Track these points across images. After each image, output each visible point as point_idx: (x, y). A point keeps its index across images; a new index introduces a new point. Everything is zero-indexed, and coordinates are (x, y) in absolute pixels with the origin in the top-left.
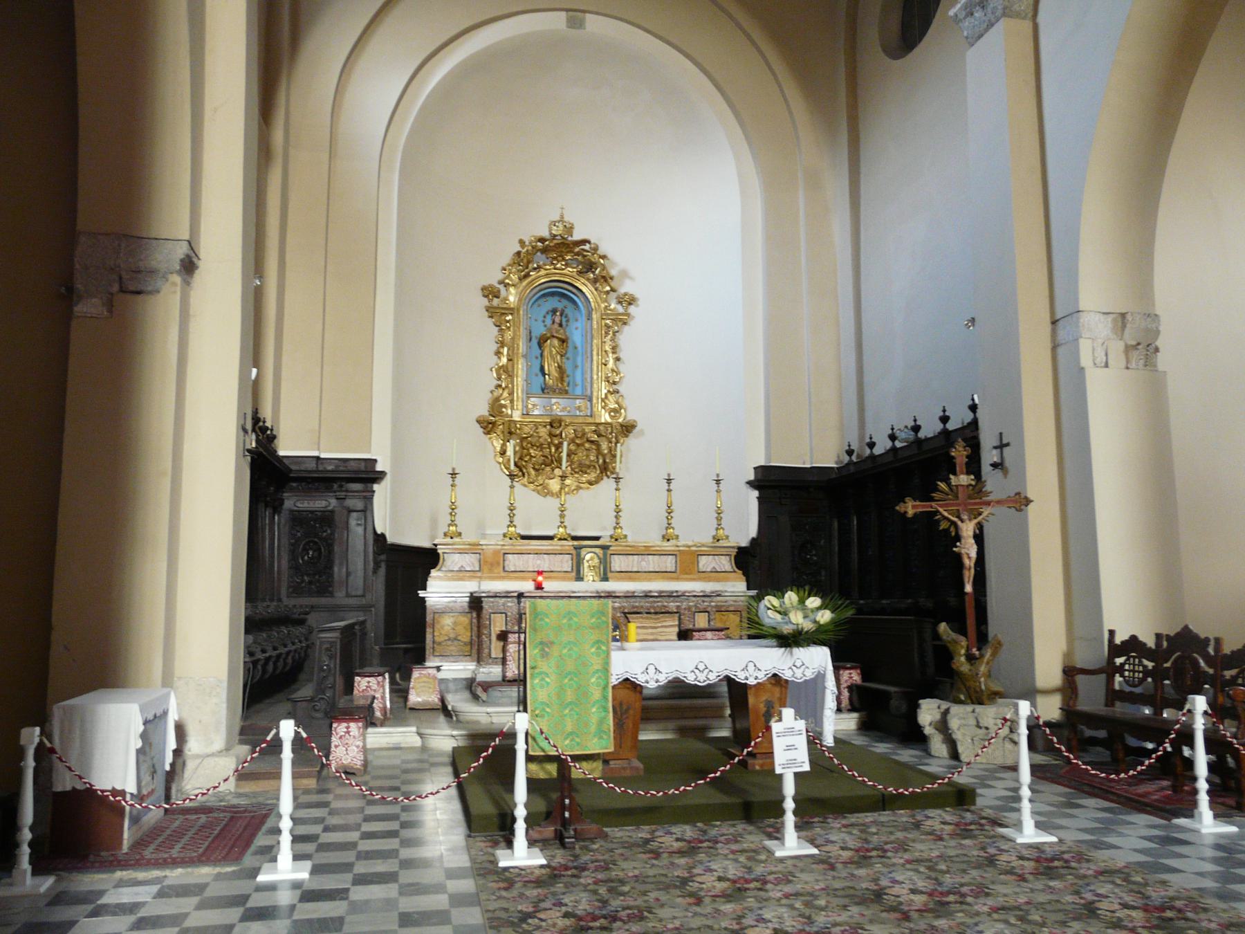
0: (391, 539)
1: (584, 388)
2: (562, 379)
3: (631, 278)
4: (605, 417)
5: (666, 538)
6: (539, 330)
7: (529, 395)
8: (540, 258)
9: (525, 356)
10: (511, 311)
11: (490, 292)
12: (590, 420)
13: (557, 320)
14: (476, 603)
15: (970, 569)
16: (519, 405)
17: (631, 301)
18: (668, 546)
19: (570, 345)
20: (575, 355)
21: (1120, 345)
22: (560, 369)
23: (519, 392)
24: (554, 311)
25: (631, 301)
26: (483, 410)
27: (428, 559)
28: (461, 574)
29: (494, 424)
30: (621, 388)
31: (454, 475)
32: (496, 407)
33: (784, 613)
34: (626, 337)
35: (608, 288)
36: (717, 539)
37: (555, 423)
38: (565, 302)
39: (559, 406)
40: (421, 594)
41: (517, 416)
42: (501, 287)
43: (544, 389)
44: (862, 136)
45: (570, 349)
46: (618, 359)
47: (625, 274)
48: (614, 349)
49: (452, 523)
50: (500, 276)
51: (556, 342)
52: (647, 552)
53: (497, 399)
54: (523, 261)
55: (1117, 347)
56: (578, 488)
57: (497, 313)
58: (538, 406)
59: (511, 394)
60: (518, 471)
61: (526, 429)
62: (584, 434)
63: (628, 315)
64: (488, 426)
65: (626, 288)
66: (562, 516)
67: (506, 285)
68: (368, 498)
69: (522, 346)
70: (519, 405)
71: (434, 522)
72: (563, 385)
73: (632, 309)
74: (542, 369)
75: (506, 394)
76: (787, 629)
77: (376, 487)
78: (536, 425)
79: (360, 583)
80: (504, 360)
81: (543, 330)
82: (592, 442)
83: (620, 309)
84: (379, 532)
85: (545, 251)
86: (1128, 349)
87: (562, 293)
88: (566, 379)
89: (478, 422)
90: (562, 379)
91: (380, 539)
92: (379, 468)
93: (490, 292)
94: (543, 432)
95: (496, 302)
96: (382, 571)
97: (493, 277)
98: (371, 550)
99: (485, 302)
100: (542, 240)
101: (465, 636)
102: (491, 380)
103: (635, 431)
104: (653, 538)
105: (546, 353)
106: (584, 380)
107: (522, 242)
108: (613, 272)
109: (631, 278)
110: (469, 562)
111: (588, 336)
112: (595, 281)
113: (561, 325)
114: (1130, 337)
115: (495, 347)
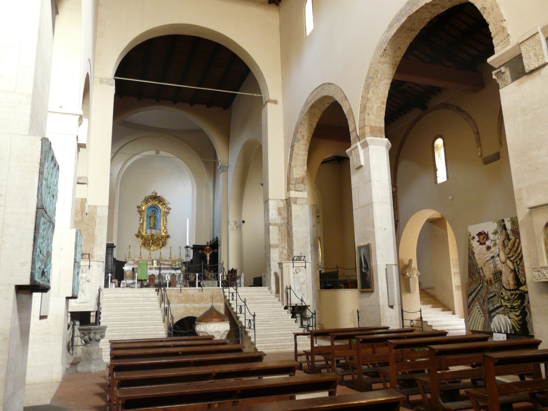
0: (117, 259)
1: (159, 228)
2: (154, 226)
3: (170, 204)
4: (163, 234)
5: (170, 258)
6: (150, 215)
7: (147, 229)
8: (150, 200)
9: (146, 221)
10: (143, 211)
11: (139, 207)
12: (160, 235)
13: (154, 213)
14: (133, 269)
15: (41, 237)
16: (144, 231)
17: (170, 209)
18: (170, 260)
19: (156, 218)
20: (158, 220)
21: (236, 227)
22: (154, 224)
23: (144, 229)
24: (153, 211)
25: (170, 209)
26: (137, 233)
27: (123, 264)
28: (131, 264)
29: (139, 236)
30: (167, 228)
31: (130, 246)
32: (139, 232)
33: (176, 266)
34: (169, 217)
35: (165, 206)
36: (179, 258)
37: (152, 235)
38: (155, 209)
39: (154, 231)
40: (123, 268)
41: (144, 234)
42: (141, 206)
43: (151, 228)
44: (216, 179)
45: (157, 219)
46: (167, 222)
47: (169, 203)
48: (166, 219)
49: (129, 255)
50: (141, 203)
51: (153, 218)
52: (166, 261)
53: (140, 230)
54: (146, 200)
55: (235, 227)
56: (157, 249)
57: (140, 212)
58: (149, 231)
59: (143, 229)
60: (144, 244)
61: (146, 237)
62: (158, 238)
63: (169, 212)
64: (137, 236)
65: (169, 206)
66: (150, 254)
67: (142, 206)
68: (112, 251)
69: (145, 218)
70: (144, 231)
71: (126, 256)
72: (154, 227)
73: (170, 211)
74: (150, 223)
75: (142, 229)
76: (176, 268)
77: (114, 249)
78: (148, 236)
79: (110, 267)
80: (142, 222)
81: (150, 215)
82: (160, 240)
83: (167, 211)
84: (114, 258)
85: (151, 198)
86: (237, 227)
87: (154, 209)
88: (155, 226)
89: (136, 235)
90: (154, 226)
91: (115, 259)
92: (114, 245)
93: (139, 207)
94: (150, 237)
95: (140, 209)
96: (115, 265)
97: (139, 204)
98: (113, 261)
99: (138, 209)
100: (150, 196)
101: (131, 276)
102: (138, 226)
103: (170, 237)
104: (167, 258)
105: (151, 220)
106: (159, 226)
107: (146, 197)
108: (166, 203)
109: (170, 204)
110: (132, 262)
111: (160, 217)
112: (162, 205)
113: (154, 214)
114: (237, 225)
115: (139, 219)
